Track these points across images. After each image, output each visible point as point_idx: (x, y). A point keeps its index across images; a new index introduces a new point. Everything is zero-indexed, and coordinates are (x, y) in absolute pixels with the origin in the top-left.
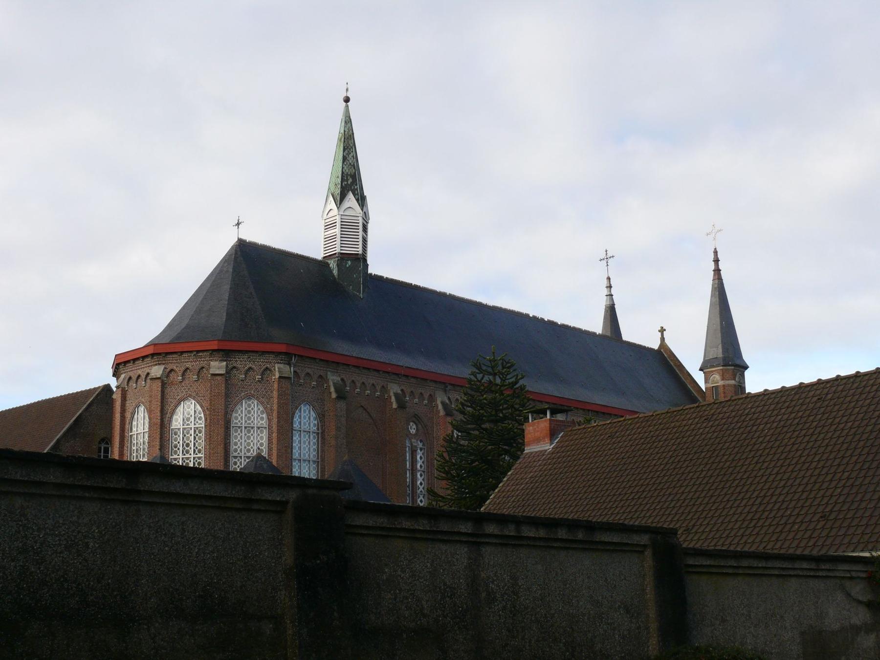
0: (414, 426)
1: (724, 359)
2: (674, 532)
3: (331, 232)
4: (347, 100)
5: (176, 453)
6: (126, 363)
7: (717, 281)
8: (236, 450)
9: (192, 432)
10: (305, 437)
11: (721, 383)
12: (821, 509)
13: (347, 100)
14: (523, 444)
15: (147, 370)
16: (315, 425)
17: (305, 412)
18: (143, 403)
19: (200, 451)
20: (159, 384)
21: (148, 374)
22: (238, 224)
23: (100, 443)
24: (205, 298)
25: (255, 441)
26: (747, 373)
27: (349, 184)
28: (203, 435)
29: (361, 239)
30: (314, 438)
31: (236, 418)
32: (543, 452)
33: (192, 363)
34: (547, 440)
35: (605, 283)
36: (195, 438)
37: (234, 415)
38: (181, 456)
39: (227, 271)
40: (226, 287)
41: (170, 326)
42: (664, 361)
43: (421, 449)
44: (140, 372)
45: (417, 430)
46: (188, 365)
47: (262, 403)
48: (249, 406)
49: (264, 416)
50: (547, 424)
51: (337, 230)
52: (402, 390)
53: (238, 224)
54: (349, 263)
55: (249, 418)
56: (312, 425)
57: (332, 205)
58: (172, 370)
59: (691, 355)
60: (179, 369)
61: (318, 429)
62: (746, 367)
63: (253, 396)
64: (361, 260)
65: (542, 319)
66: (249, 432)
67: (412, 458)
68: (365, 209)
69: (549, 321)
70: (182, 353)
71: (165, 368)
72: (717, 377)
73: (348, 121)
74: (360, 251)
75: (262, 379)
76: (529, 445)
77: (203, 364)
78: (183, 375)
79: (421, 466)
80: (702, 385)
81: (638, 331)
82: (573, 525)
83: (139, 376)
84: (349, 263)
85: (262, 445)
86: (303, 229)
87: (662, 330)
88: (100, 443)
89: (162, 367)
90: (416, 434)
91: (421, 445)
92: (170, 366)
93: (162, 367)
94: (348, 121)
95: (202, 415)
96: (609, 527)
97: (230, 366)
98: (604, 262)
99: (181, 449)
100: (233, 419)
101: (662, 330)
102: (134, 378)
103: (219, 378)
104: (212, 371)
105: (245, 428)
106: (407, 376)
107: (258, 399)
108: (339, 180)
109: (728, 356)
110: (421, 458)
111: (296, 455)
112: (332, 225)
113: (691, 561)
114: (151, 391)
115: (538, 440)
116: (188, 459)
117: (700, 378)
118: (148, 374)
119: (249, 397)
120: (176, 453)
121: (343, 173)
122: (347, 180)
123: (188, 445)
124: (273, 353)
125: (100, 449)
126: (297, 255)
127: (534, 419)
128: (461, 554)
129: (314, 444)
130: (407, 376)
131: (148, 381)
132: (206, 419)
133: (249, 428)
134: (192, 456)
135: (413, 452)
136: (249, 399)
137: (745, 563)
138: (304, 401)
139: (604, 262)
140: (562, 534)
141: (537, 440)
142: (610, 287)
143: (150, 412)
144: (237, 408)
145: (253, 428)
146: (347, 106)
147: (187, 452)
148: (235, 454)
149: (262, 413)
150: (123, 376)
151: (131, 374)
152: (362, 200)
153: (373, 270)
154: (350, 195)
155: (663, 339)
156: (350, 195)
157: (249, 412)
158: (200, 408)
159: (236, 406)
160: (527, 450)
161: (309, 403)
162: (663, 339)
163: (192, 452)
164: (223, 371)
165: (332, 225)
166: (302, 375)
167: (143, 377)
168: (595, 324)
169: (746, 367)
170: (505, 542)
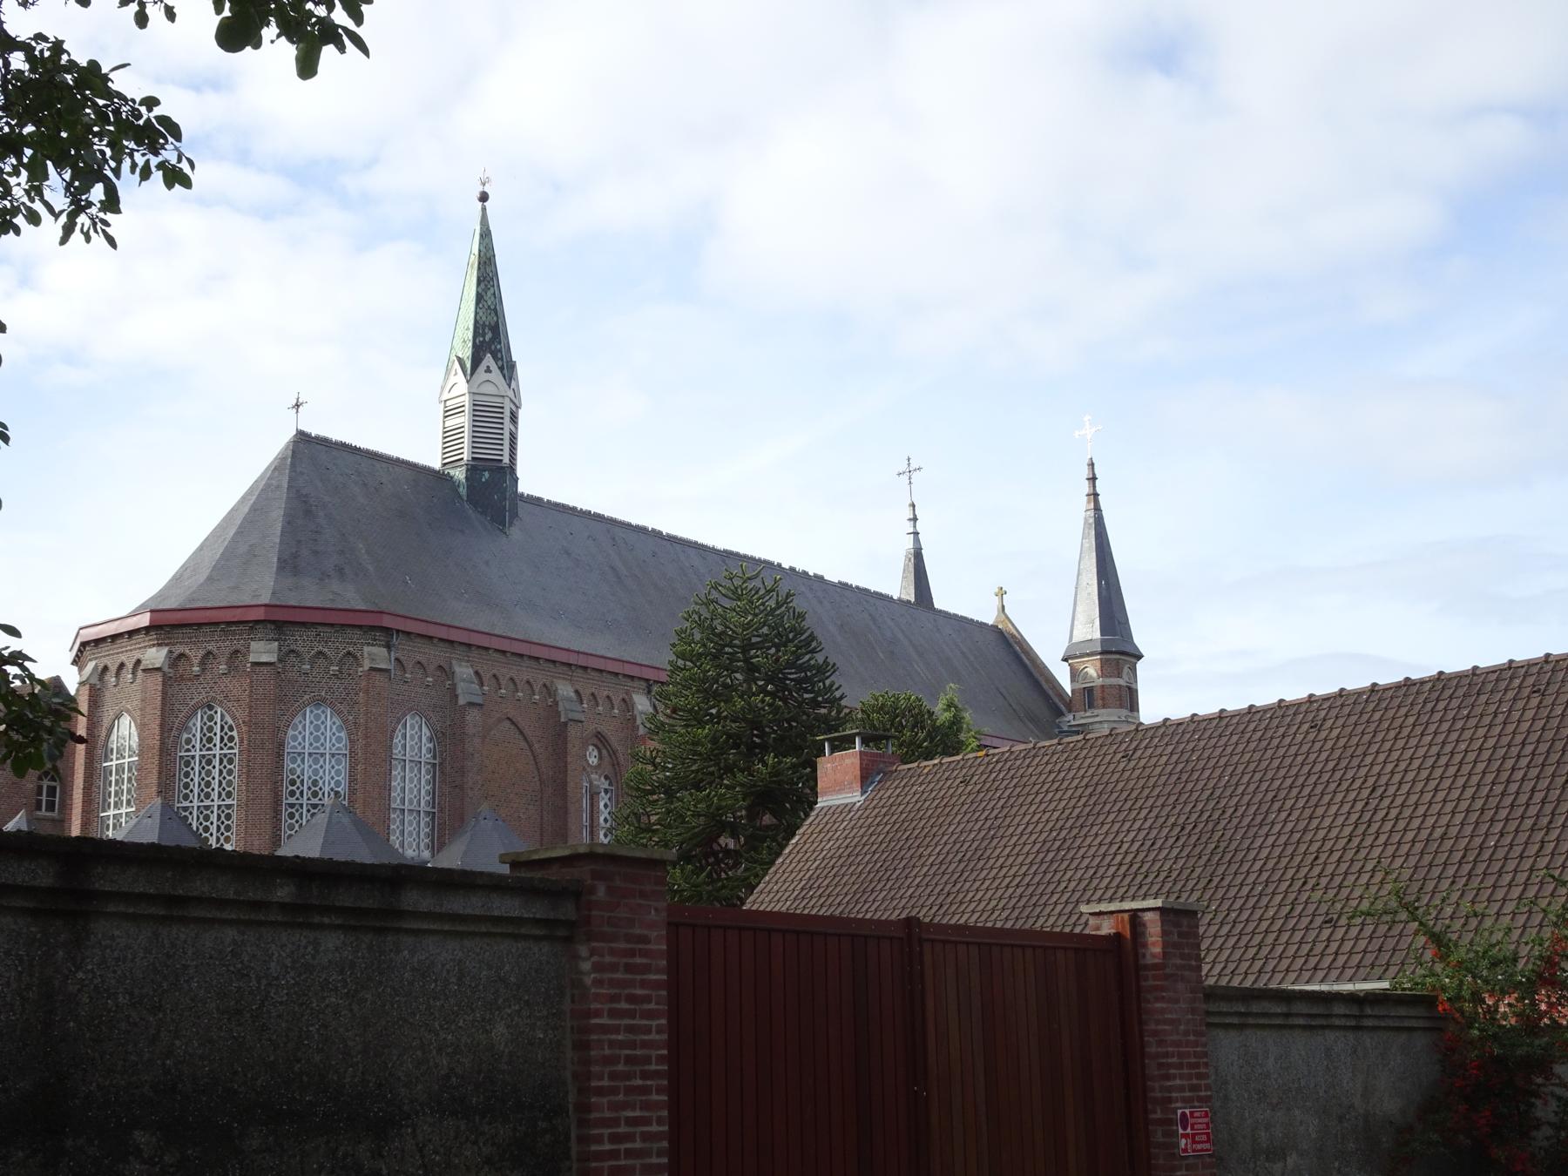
0: (596, 753)
1: (1103, 641)
3: (450, 423)
4: (484, 197)
5: (186, 797)
6: (98, 642)
7: (1092, 513)
9: (216, 762)
10: (412, 770)
12: (1324, 908)
13: (484, 197)
14: (816, 795)
15: (137, 655)
16: (429, 750)
17: (412, 727)
18: (128, 711)
19: (229, 795)
20: (159, 678)
21: (138, 662)
22: (297, 406)
23: (40, 778)
24: (239, 533)
25: (327, 778)
26: (1140, 665)
27: (489, 342)
29: (507, 436)
30: (428, 772)
31: (295, 738)
32: (848, 808)
33: (220, 646)
34: (857, 786)
36: (221, 772)
37: (291, 732)
38: (196, 803)
39: (278, 487)
40: (277, 515)
41: (177, 579)
42: (1008, 647)
43: (606, 791)
44: (123, 658)
45: (601, 758)
46: (211, 647)
47: (339, 713)
48: (317, 717)
49: (342, 734)
50: (857, 761)
51: (464, 420)
52: (577, 692)
53: (297, 406)
54: (487, 474)
55: (317, 739)
56: (424, 750)
57: (460, 379)
58: (182, 655)
60: (196, 655)
61: (434, 757)
62: (1139, 657)
63: (324, 700)
65: (819, 579)
66: (316, 761)
67: (592, 805)
68: (513, 384)
69: (816, 576)
70: (200, 625)
71: (170, 652)
73: (486, 235)
74: (506, 460)
75: (340, 671)
76: (825, 793)
77: (239, 645)
78: (202, 663)
79: (606, 820)
80: (1067, 685)
81: (961, 594)
83: (122, 665)
84: (487, 474)
85: (338, 784)
86: (414, 427)
87: (1001, 593)
88: (40, 778)
89: (165, 651)
90: (599, 766)
91: (606, 785)
92: (179, 649)
93: (165, 651)
94: (486, 235)
95: (235, 733)
97: (285, 649)
98: (905, 478)
99: (196, 791)
100: (288, 739)
101: (1001, 593)
102: (113, 668)
103: (265, 670)
104: (252, 658)
105: (333, 755)
107: (332, 706)
108: (470, 335)
109: (1117, 648)
110: (606, 806)
111: (424, 819)
112: (458, 410)
114: (144, 691)
115: (839, 782)
116: (207, 807)
118: (138, 662)
119: (319, 702)
120: (186, 797)
121: (476, 322)
122: (484, 335)
123: (208, 784)
124: (360, 627)
125: (40, 788)
126: (398, 460)
127: (832, 751)
129: (428, 782)
131: (140, 673)
132: (241, 741)
133: (316, 756)
134: (216, 803)
135: (594, 796)
136: (318, 706)
138: (411, 709)
139: (905, 478)
141: (839, 787)
142: (915, 519)
143: (142, 727)
144: (296, 720)
145: (322, 755)
146: (484, 209)
147: (208, 796)
148: (292, 800)
149: (340, 729)
150: (90, 666)
151: (106, 661)
152: (508, 369)
154: (488, 360)
156: (488, 360)
157: (317, 728)
158: (230, 722)
160: (822, 803)
161: (421, 714)
163: (215, 795)
164: (272, 658)
165: (458, 410)
166: (409, 666)
167: (130, 666)
168: (893, 583)
169: (1139, 657)
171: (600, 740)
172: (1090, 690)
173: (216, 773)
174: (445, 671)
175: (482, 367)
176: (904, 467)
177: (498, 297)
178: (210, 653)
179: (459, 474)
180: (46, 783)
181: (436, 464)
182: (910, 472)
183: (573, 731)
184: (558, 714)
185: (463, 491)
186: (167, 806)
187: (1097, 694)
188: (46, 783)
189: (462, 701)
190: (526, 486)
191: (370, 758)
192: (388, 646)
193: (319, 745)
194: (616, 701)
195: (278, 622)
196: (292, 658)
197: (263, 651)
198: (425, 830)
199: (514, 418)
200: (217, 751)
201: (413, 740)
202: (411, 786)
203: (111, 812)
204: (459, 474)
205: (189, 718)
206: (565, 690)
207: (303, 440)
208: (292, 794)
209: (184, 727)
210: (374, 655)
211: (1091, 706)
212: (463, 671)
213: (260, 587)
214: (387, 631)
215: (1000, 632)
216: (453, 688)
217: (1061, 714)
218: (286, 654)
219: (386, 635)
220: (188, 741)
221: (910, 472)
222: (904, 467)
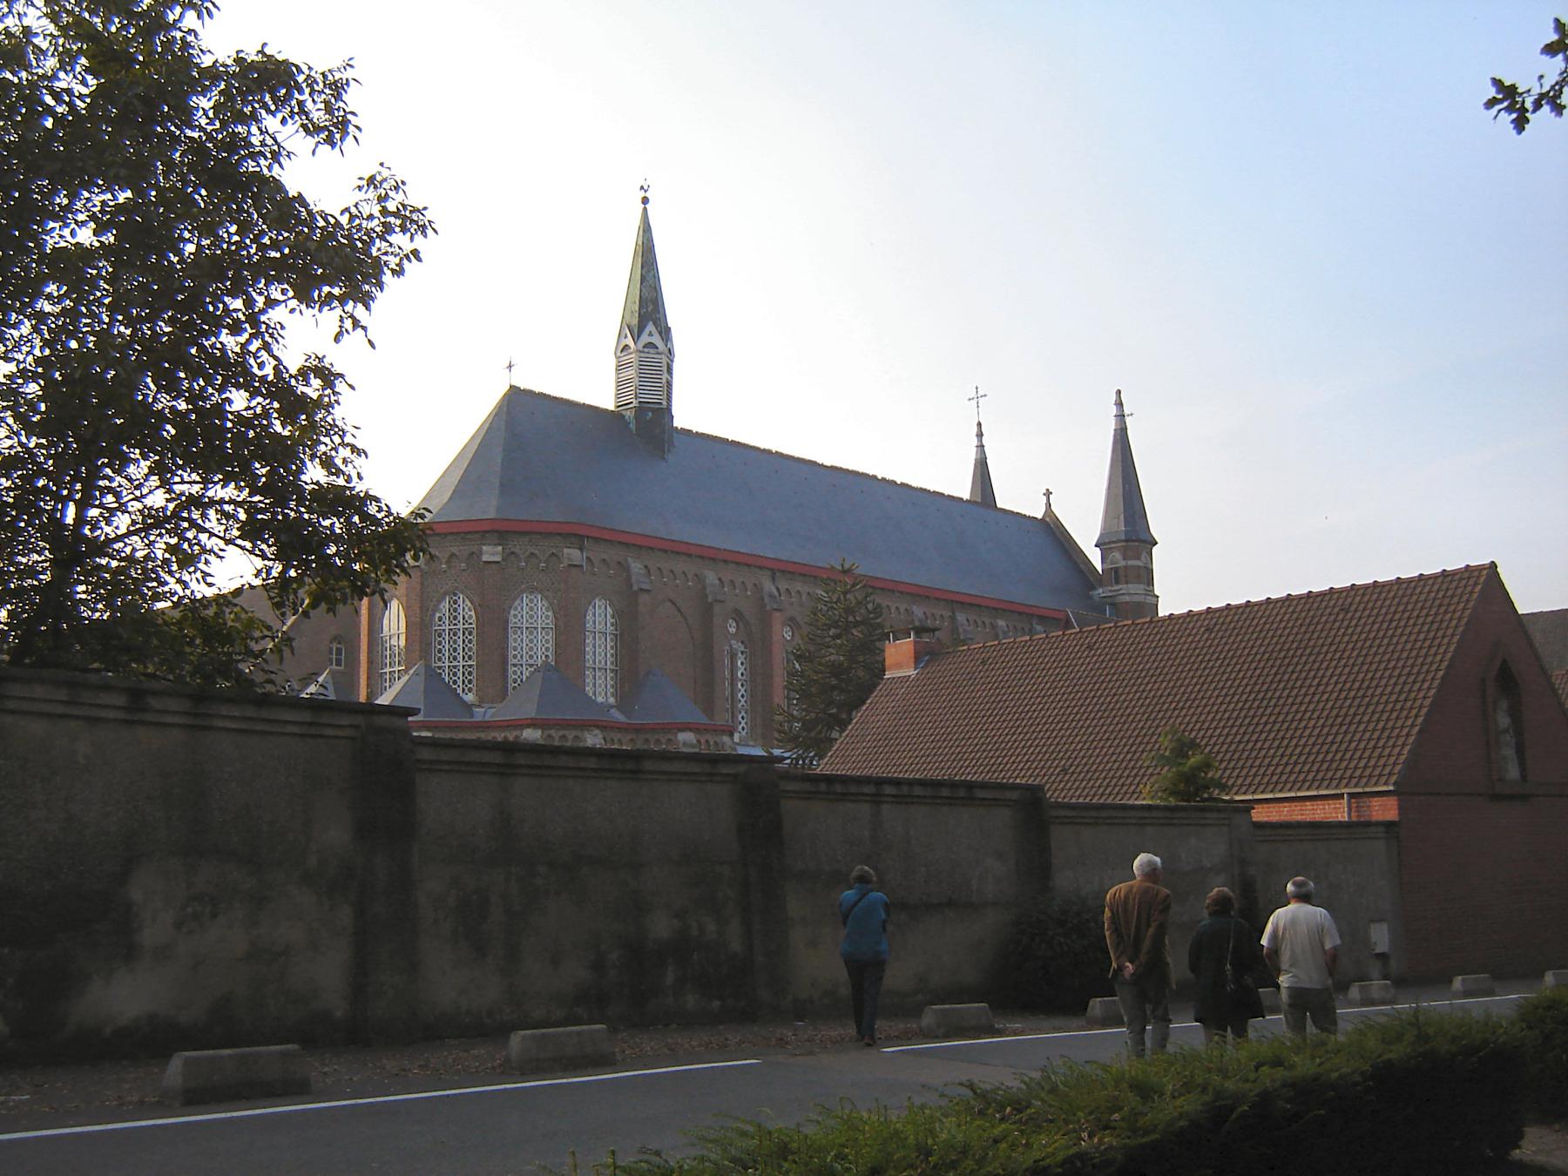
1: (1126, 533)
2: (1040, 788)
8: (515, 657)
11: (1122, 563)
13: (645, 201)
28: (473, 638)
35: (975, 429)
42: (1051, 530)
46: (454, 550)
50: (912, 647)
59: (1086, 528)
64: (665, 412)
72: (1117, 555)
77: (475, 549)
81: (1017, 495)
82: (954, 785)
86: (593, 381)
87: (1048, 493)
96: (984, 786)
101: (1048, 493)
104: (485, 558)
106: (725, 561)
111: (610, 675)
112: (628, 365)
113: (1054, 813)
115: (899, 658)
117: (1095, 557)
119: (533, 590)
128: (865, 809)
130: (725, 561)
137: (1104, 814)
140: (945, 792)
141: (899, 666)
152: (665, 333)
153: (679, 422)
154: (650, 327)
155: (1049, 505)
156: (650, 327)
159: (514, 600)
162: (1049, 505)
168: (961, 487)
170: (899, 800)
171: (738, 616)
172: (1116, 570)
173: (460, 642)
174: (623, 566)
175: (647, 331)
176: (973, 394)
177: (657, 278)
178: (453, 555)
179: (629, 415)
180: (335, 646)
181: (611, 406)
182: (978, 397)
183: (717, 609)
184: (706, 596)
185: (633, 426)
186: (428, 667)
187: (1121, 573)
188: (335, 646)
189: (635, 588)
190: (679, 422)
191: (569, 632)
192: (581, 549)
193: (532, 627)
194: (749, 586)
195: (500, 532)
196: (512, 558)
197: (491, 553)
198: (610, 652)
199: (670, 370)
200: (461, 626)
201: (600, 617)
202: (600, 651)
203: (388, 670)
204: (629, 415)
205: (439, 602)
206: (711, 577)
207: (514, 391)
208: (515, 657)
209: (436, 609)
210: (573, 554)
211: (1117, 582)
212: (636, 567)
213: (487, 508)
214: (581, 537)
215: (1047, 524)
216: (629, 578)
217: (1094, 588)
218: (509, 555)
219: (577, 537)
220: (440, 619)
221: (978, 397)
222: (973, 394)
